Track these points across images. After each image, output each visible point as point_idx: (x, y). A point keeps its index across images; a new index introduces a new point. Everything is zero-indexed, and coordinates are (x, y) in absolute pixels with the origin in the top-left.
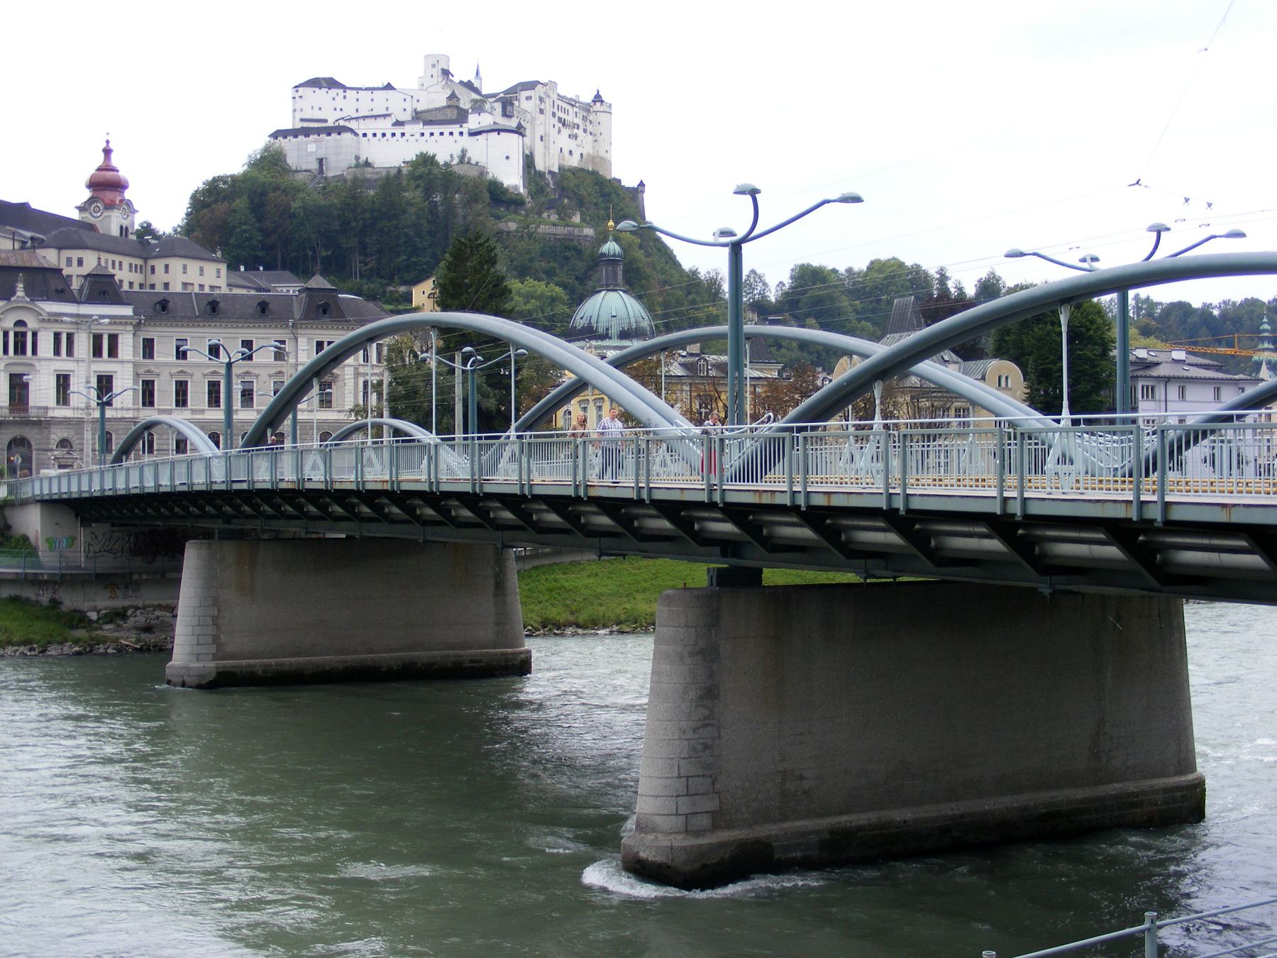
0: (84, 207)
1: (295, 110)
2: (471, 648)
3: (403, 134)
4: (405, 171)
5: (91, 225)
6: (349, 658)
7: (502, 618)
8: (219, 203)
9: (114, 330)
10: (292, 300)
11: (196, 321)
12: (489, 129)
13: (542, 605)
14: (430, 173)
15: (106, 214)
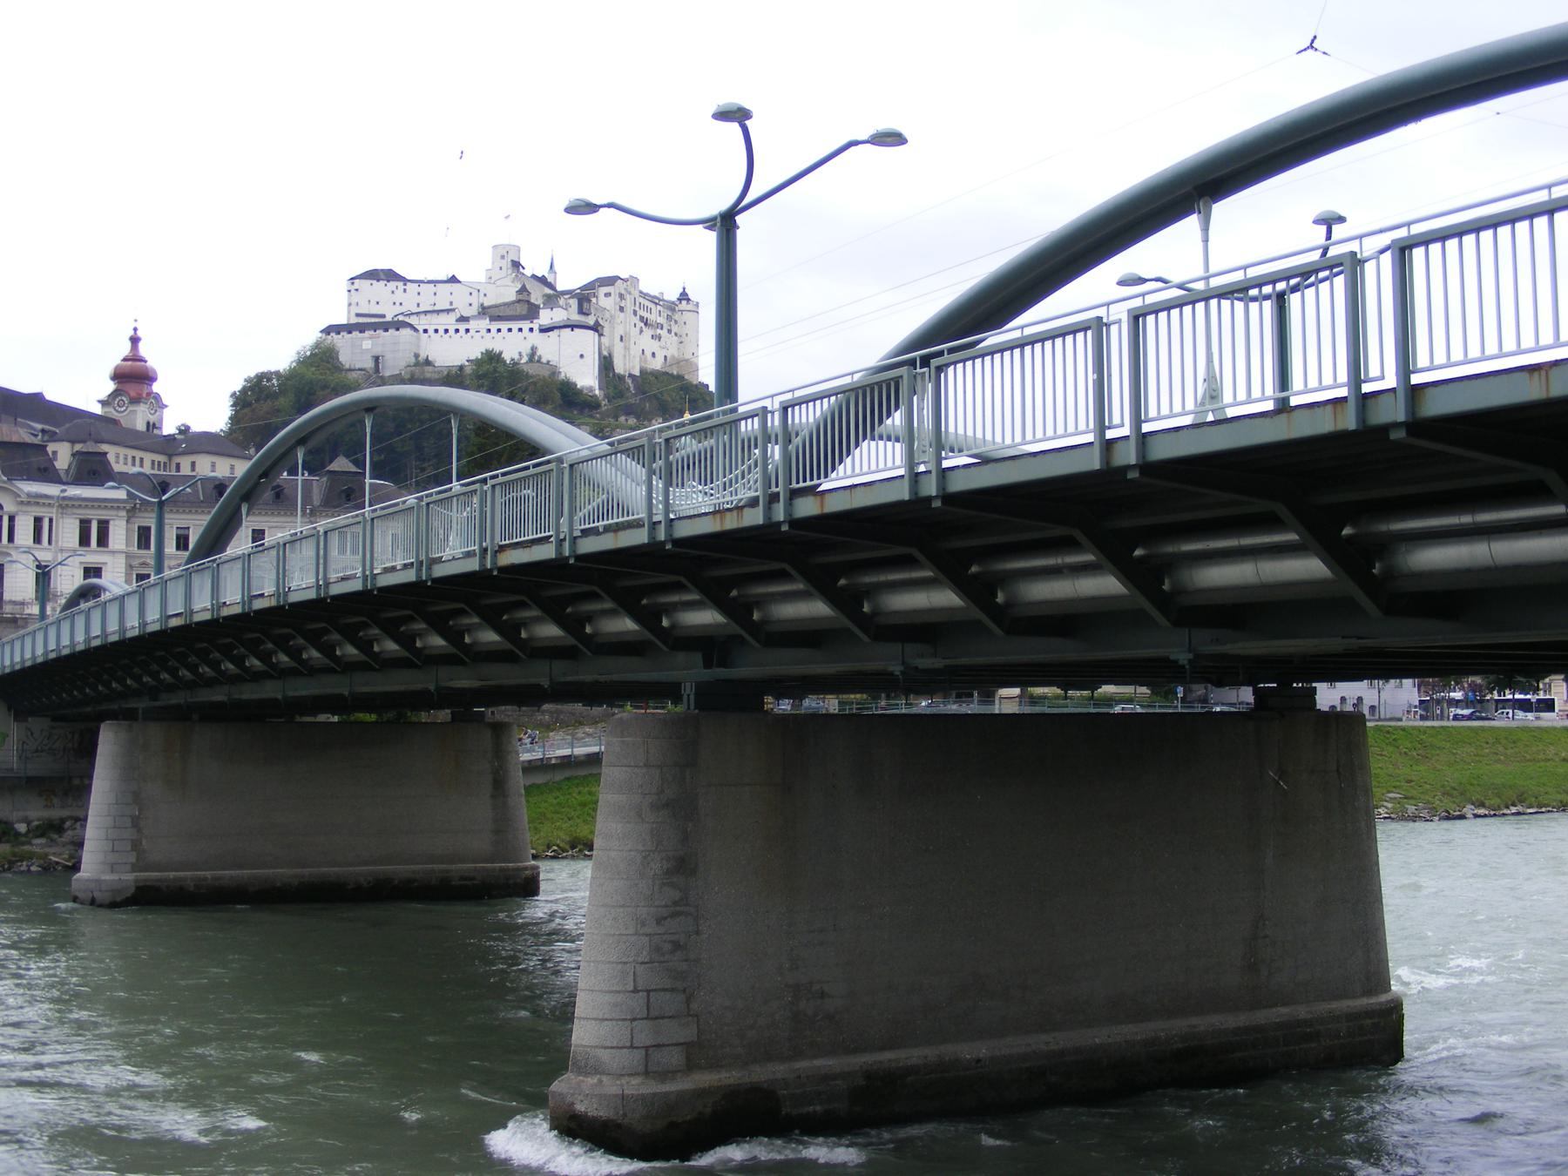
0: (107, 401)
1: (350, 305)
2: (463, 861)
3: (467, 331)
4: (468, 370)
5: (115, 420)
6: (307, 871)
7: (503, 825)
8: (262, 402)
9: (104, 514)
10: (312, 485)
11: (200, 507)
12: (562, 324)
13: (571, 822)
14: (495, 370)
15: (130, 408)
